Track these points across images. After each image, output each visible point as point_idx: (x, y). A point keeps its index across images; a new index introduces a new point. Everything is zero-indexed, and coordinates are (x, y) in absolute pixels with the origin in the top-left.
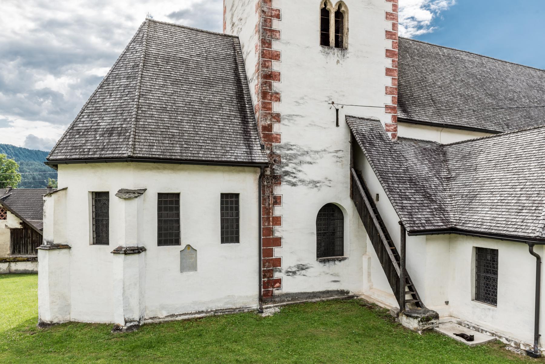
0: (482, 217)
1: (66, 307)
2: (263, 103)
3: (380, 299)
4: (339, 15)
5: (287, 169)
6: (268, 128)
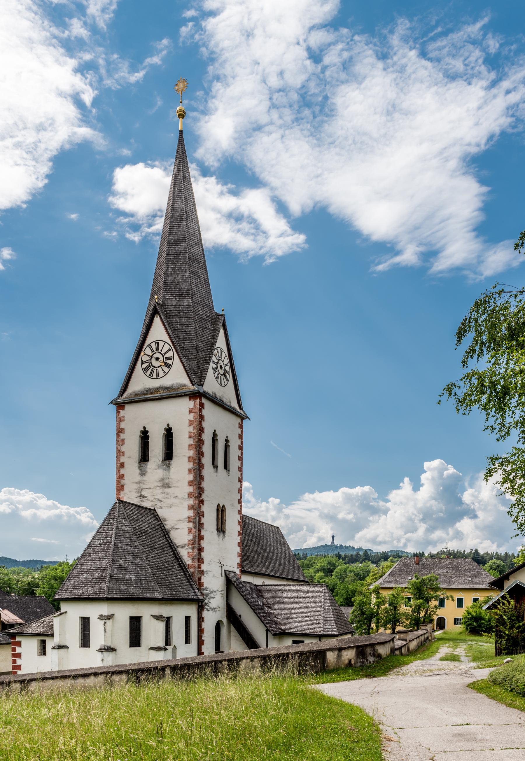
6: (200, 579)
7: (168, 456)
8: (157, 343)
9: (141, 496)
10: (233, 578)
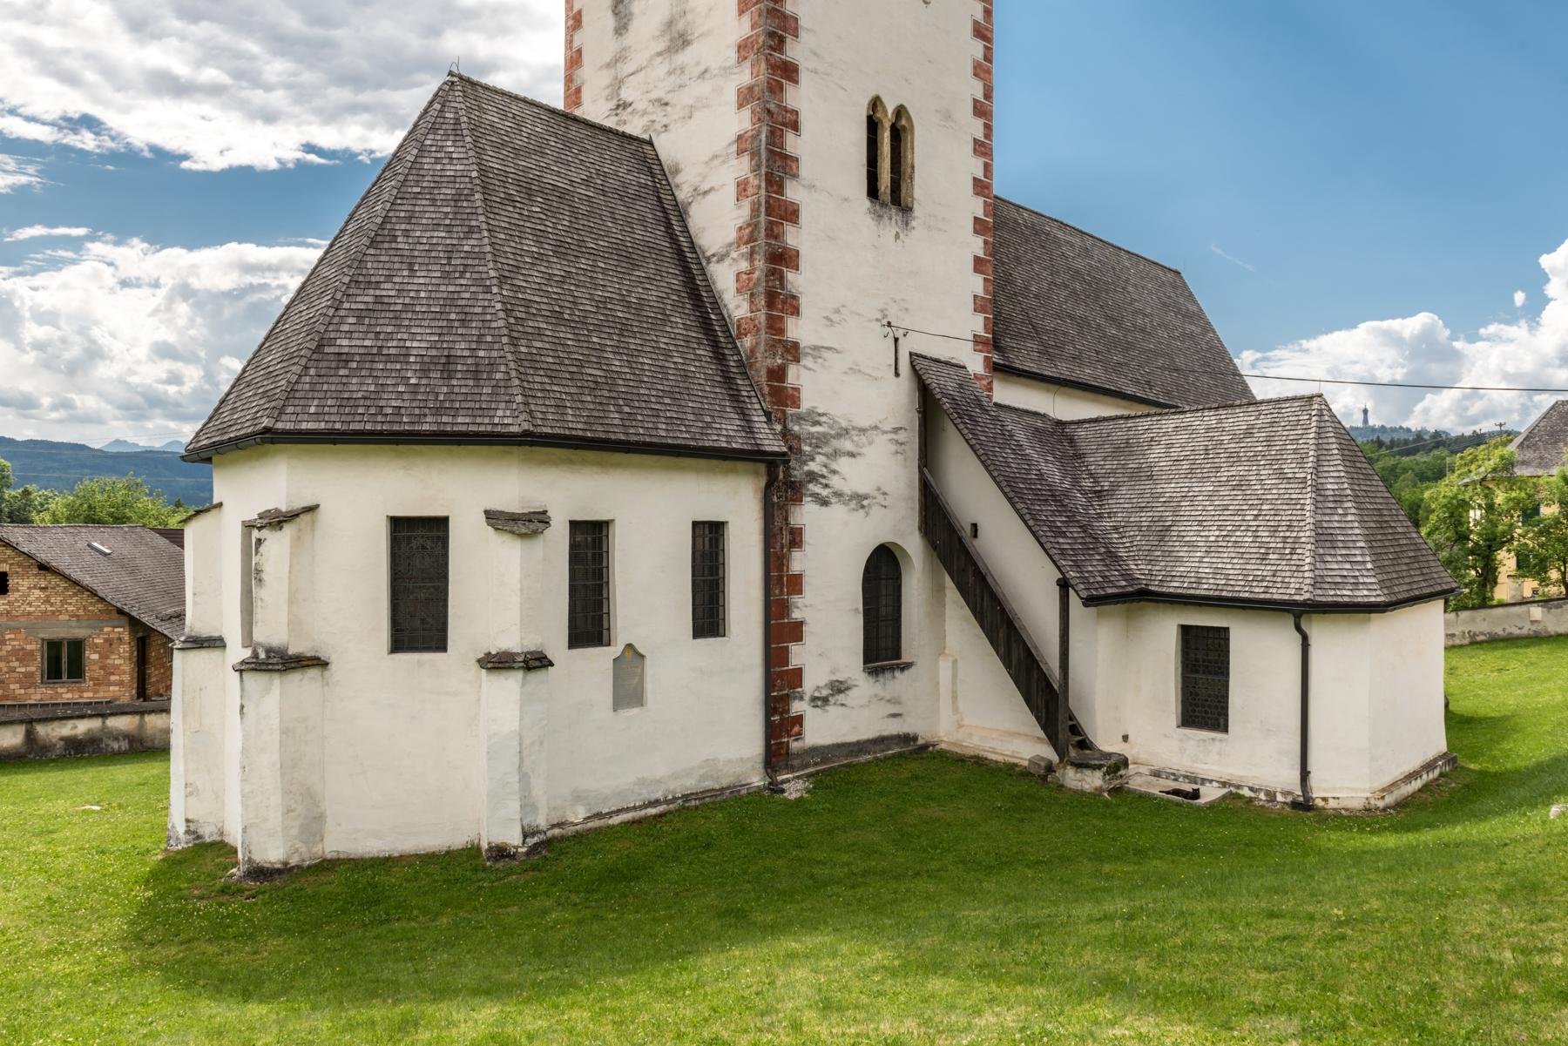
0: (1198, 564)
1: (314, 824)
2: (769, 317)
3: (986, 745)
4: (898, 134)
5: (812, 466)
6: (778, 374)
10: (941, 382)
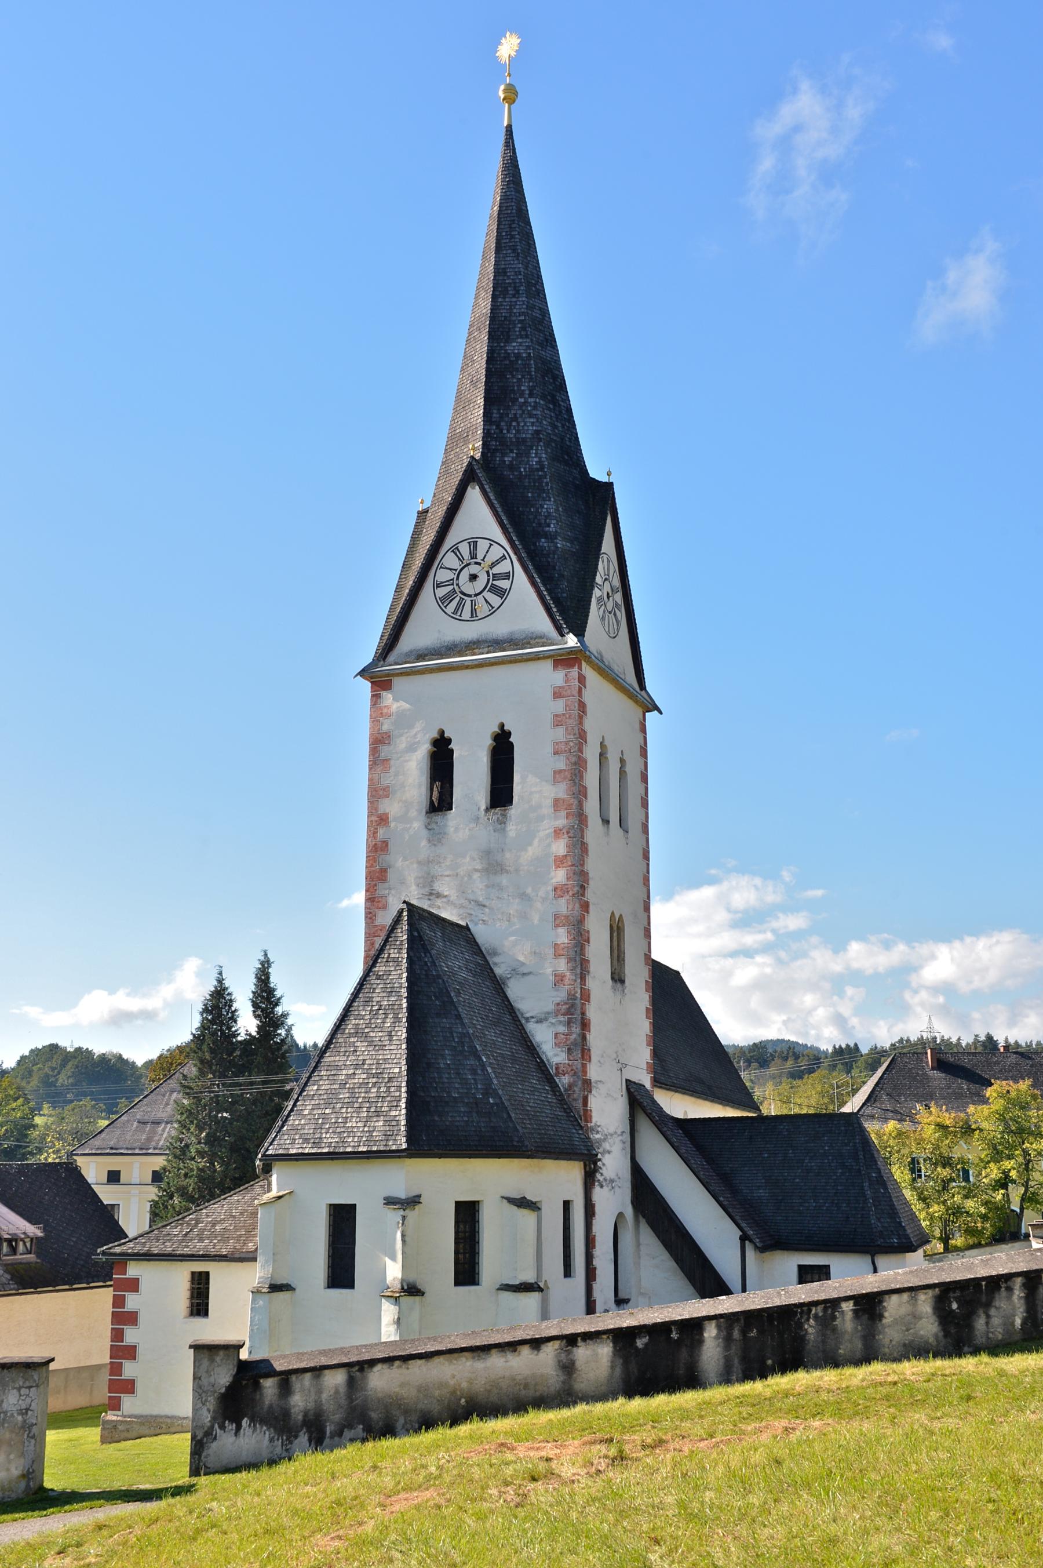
7: (501, 793)
8: (473, 544)
9: (431, 894)
